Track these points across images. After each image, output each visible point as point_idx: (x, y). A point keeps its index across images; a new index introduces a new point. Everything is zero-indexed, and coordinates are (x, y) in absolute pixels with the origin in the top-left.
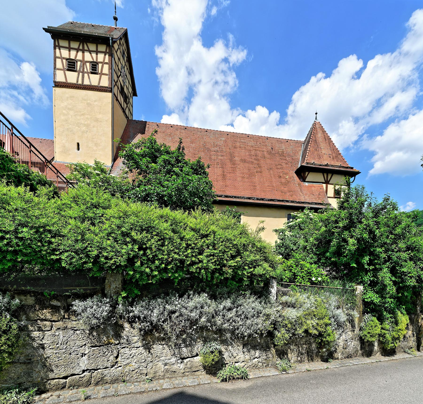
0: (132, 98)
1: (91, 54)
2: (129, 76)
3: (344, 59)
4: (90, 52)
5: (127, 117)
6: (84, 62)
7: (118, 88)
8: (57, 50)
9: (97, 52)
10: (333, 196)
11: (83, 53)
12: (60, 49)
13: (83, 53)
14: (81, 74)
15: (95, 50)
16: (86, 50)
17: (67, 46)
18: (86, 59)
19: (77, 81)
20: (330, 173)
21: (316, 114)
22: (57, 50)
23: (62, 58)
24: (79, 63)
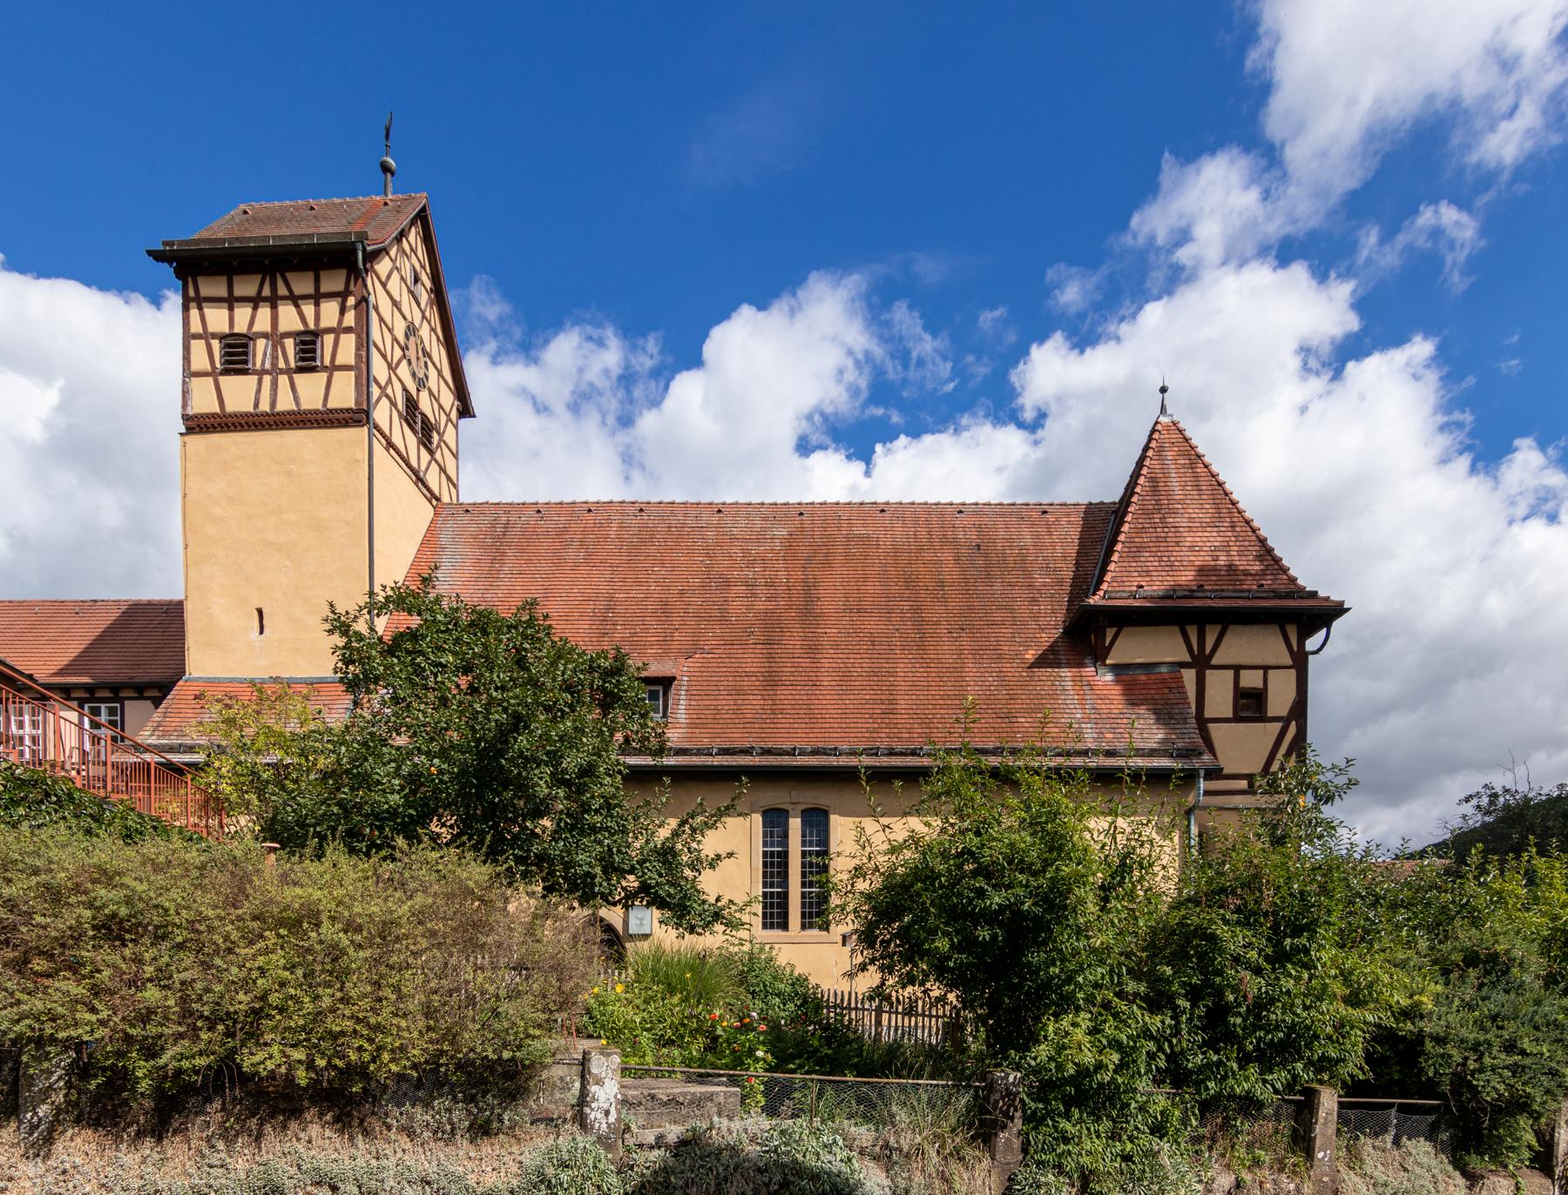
0: (456, 427)
1: (297, 306)
2: (439, 355)
3: (746, 312)
4: (295, 300)
5: (433, 497)
6: (275, 337)
7: (393, 404)
8: (194, 313)
9: (317, 298)
10: (1230, 715)
11: (274, 307)
12: (200, 308)
13: (274, 307)
14: (267, 379)
15: (310, 290)
16: (284, 298)
17: (223, 293)
18: (283, 327)
19: (256, 405)
20: (1213, 622)
21: (1163, 390)
22: (194, 313)
23: (206, 336)
24: (261, 344)
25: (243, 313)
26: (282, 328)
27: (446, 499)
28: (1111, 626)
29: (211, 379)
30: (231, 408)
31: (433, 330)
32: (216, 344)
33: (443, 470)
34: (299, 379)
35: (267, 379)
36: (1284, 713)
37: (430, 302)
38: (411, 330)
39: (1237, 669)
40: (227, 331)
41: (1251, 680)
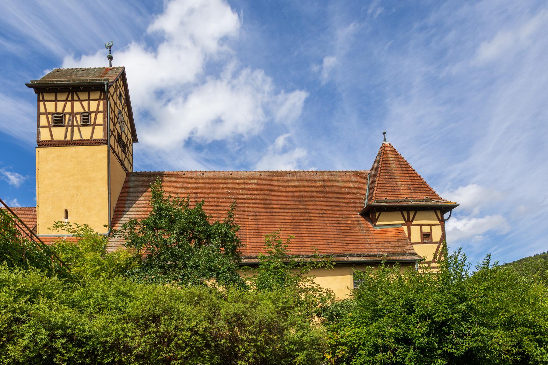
2: (127, 120)
5: (126, 170)
7: (115, 138)
14: (69, 128)
17: (53, 98)
21: (384, 134)
25: (60, 105)
26: (75, 111)
27: (130, 171)
28: (377, 212)
29: (48, 129)
30: (84, 138)
31: (125, 112)
32: (50, 116)
33: (129, 160)
34: (82, 129)
35: (69, 128)
36: (438, 240)
37: (125, 103)
38: (120, 112)
39: (421, 225)
40: (54, 111)
41: (426, 229)
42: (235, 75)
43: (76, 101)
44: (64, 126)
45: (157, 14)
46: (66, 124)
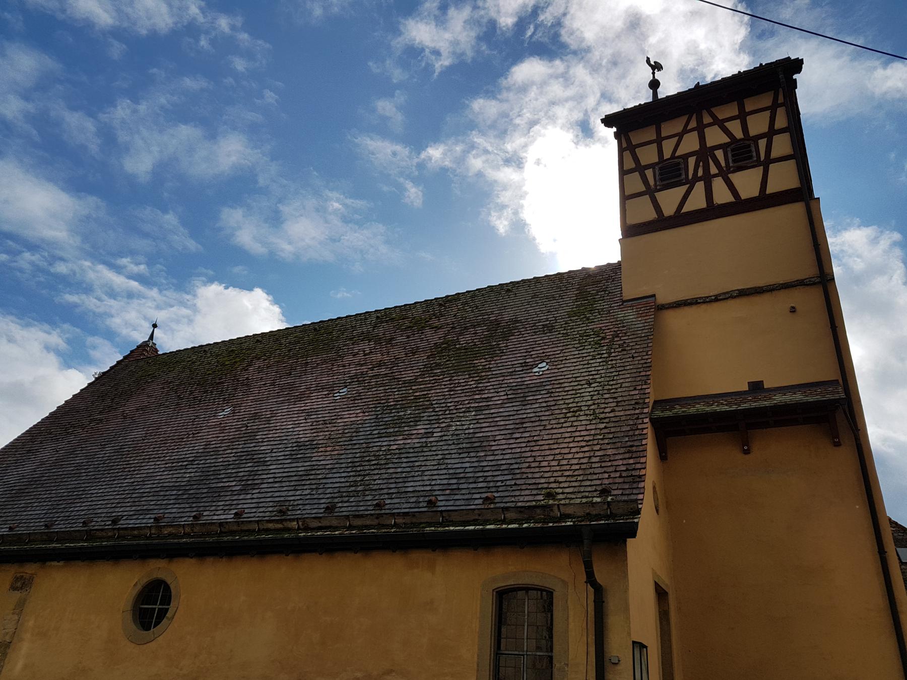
30: (744, 195)
42: (514, 84)
43: (710, 125)
44: (758, 163)
45: (190, 282)
46: (762, 158)
